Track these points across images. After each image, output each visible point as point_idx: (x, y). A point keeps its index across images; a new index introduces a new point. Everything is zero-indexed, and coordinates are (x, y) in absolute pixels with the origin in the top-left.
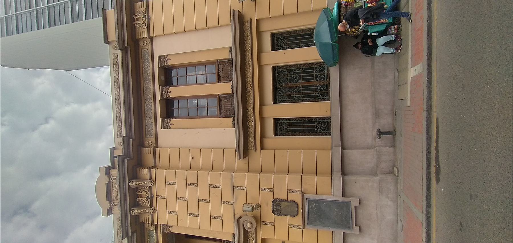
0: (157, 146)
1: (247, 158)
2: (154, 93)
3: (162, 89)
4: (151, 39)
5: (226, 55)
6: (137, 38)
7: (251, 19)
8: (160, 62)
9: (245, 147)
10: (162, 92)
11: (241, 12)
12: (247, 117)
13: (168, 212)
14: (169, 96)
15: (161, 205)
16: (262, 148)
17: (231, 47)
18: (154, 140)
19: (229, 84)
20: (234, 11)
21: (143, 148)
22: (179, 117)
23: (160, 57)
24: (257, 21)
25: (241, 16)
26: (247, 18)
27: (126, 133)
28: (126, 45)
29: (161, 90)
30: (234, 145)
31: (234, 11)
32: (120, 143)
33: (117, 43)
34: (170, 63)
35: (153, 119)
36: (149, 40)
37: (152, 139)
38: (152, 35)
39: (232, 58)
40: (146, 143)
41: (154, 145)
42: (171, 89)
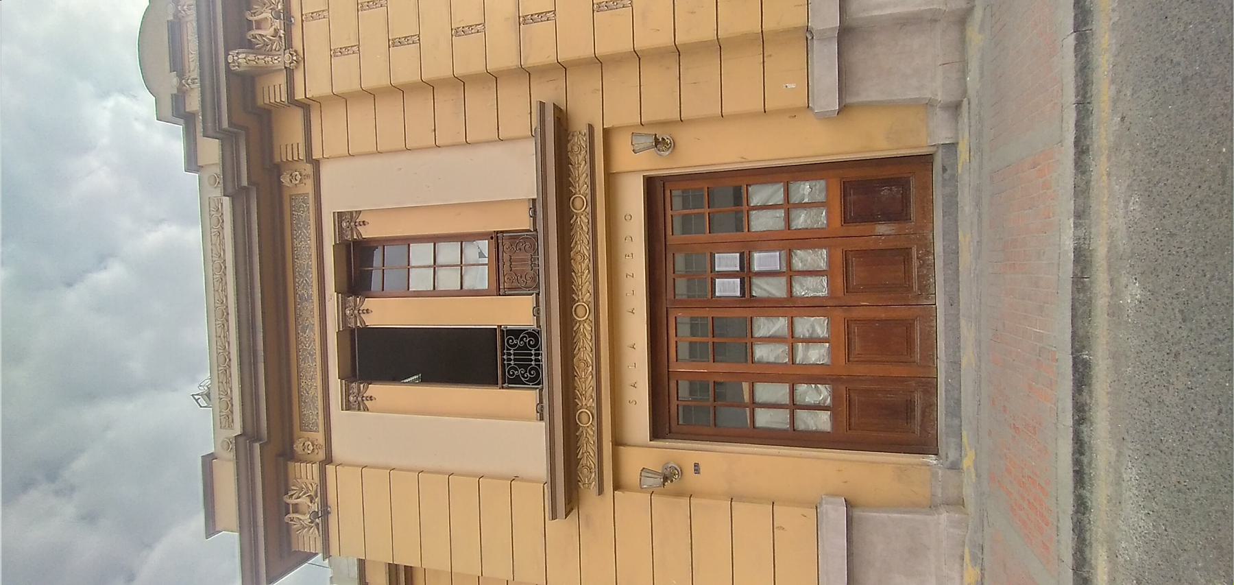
0: (329, 459)
1: (575, 511)
2: (322, 320)
3: (347, 390)
4: (316, 164)
5: (522, 222)
6: (277, 160)
7: (591, 127)
8: (340, 231)
9: (569, 486)
10: (348, 395)
11: (563, 108)
12: (570, 184)
13: (334, 53)
14: (359, 234)
15: (314, 40)
16: (617, 486)
17: (534, 200)
18: (320, 437)
19: (529, 301)
20: (542, 104)
21: (291, 464)
22: (383, 293)
23: (340, 216)
24: (607, 132)
25: (562, 120)
26: (579, 125)
27: (244, 428)
28: (245, 183)
29: (343, 306)
30: (540, 468)
31: (542, 104)
32: (212, 181)
33: (218, 170)
34: (367, 233)
35: (313, 243)
36: (309, 169)
37: (312, 435)
38: (316, 155)
39: (536, 230)
40: (298, 447)
41: (321, 455)
42: (369, 303)
